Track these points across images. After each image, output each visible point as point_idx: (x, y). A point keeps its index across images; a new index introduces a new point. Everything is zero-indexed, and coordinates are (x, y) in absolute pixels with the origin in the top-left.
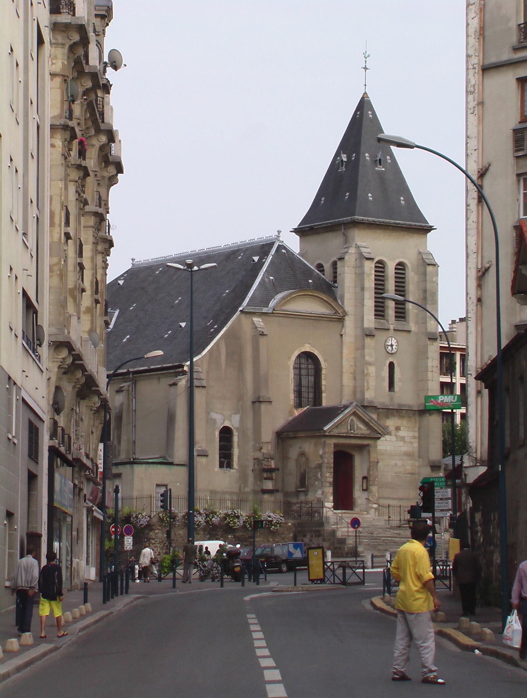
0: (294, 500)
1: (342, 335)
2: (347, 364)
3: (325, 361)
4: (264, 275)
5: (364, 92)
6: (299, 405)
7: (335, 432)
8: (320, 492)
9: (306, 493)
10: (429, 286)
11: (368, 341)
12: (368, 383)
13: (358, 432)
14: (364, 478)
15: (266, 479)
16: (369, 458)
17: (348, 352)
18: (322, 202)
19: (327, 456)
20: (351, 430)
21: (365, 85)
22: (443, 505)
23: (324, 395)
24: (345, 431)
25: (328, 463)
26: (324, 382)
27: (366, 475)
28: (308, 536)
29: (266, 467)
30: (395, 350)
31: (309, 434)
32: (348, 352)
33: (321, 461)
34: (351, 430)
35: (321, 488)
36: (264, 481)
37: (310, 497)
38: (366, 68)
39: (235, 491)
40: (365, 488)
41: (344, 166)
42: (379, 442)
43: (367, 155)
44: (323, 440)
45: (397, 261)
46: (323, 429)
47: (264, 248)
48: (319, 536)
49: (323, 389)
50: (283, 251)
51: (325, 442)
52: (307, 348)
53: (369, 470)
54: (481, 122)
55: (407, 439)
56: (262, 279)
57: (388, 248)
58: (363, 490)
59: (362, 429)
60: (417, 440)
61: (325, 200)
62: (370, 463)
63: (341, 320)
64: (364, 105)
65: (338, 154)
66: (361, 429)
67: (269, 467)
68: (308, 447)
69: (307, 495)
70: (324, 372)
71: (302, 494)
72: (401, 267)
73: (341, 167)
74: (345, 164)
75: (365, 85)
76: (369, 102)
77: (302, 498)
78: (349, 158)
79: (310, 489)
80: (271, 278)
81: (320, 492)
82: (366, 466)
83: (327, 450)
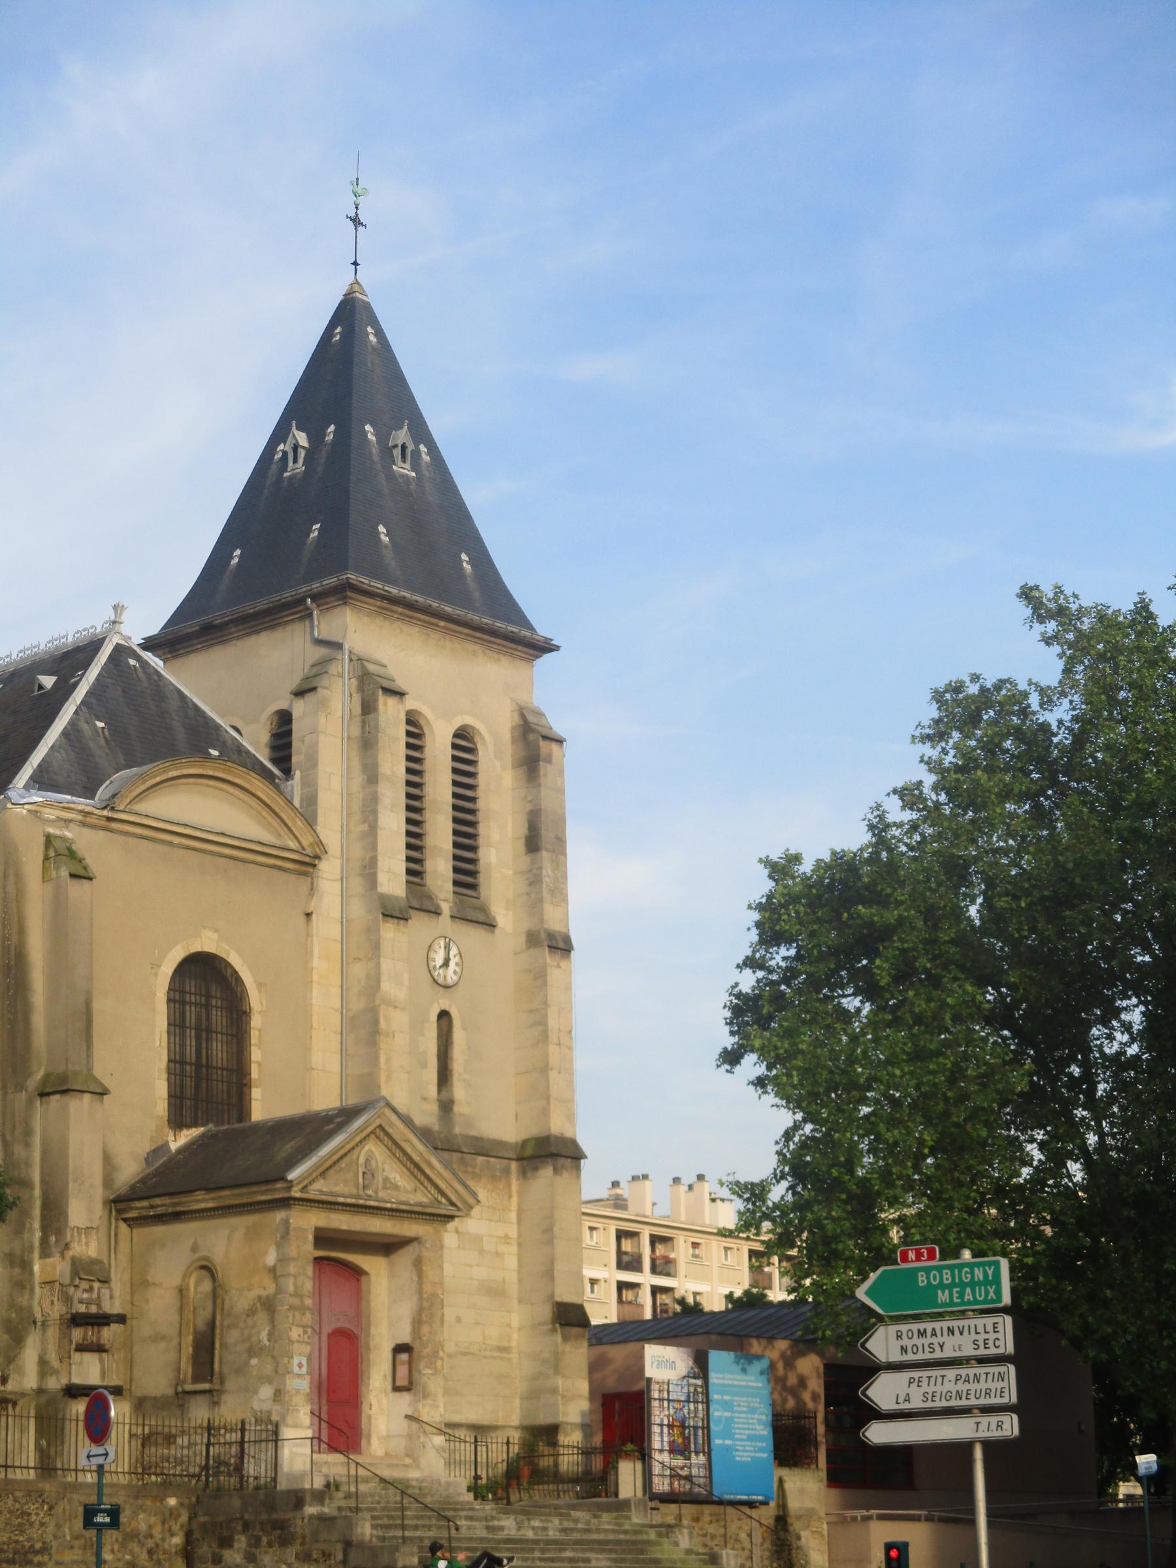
0: (172, 1423)
1: (308, 915)
2: (325, 1002)
3: (260, 986)
4: (76, 712)
5: (352, 280)
6: (177, 1121)
7: (319, 1188)
8: (266, 1392)
9: (213, 1396)
10: (547, 799)
11: (389, 932)
12: (388, 1059)
13: (390, 1198)
14: (399, 1349)
15: (81, 1348)
16: (420, 1282)
17: (324, 966)
18: (236, 560)
19: (292, 1269)
20: (365, 1187)
21: (355, 264)
22: (983, 1385)
23: (256, 1093)
24: (349, 1189)
25: (297, 1294)
26: (256, 1054)
27: (405, 1337)
28: (241, 1542)
29: (82, 1309)
30: (455, 978)
31: (228, 1197)
32: (324, 966)
33: (271, 1289)
34: (365, 1187)
35: (270, 1381)
36: (77, 1356)
37: (230, 1410)
38: (356, 221)
39: (457, 1130)
40: (402, 1381)
41: (301, 461)
42: (449, 1236)
43: (368, 428)
44: (279, 1216)
45: (457, 723)
46: (283, 1179)
47: (71, 660)
48: (285, 1542)
49: (254, 1074)
50: (132, 662)
51: (286, 1223)
52: (207, 943)
53: (417, 1323)
55: (488, 1245)
56: (72, 723)
57: (442, 680)
58: (396, 1389)
59: (400, 1186)
60: (514, 1249)
61: (241, 556)
62: (421, 1299)
63: (307, 865)
64: (351, 314)
65: (280, 433)
66: (397, 1188)
67: (93, 1309)
68: (223, 1240)
69: (216, 1404)
70: (256, 1021)
71: (201, 1399)
72: (464, 744)
73: (291, 464)
74: (302, 454)
75: (355, 264)
76: (367, 307)
77: (199, 1413)
78: (316, 438)
79: (230, 1385)
80: (101, 725)
81: (266, 1392)
82: (406, 1310)
83: (292, 1250)
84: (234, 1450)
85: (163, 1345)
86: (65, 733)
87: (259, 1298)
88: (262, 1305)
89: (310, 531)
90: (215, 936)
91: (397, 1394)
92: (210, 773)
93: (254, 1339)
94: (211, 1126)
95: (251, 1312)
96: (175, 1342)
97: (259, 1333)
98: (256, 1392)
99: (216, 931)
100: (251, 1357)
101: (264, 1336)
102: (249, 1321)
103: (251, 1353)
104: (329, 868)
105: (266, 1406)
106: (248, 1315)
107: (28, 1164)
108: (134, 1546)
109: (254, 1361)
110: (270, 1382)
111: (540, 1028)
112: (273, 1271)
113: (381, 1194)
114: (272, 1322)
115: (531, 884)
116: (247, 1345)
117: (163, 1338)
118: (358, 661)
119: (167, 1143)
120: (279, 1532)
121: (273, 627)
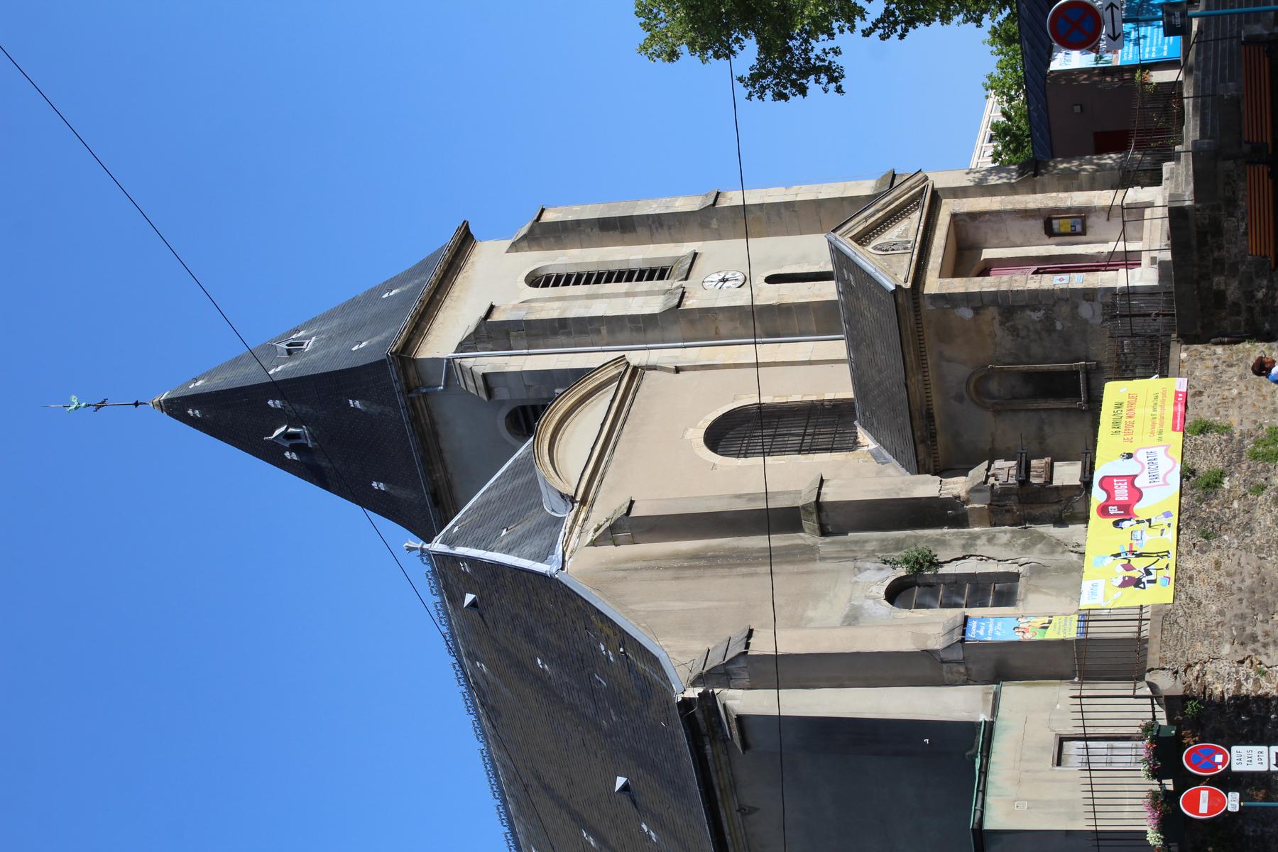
1: (678, 370)
3: (735, 399)
6: (854, 445)
28: (1218, 281)
54: (653, 563)
84: (1139, 342)
85: (1047, 429)
86: (509, 552)
87: (1002, 324)
88: (1008, 321)
89: (355, 408)
90: (691, 430)
91: (1089, 231)
92: (548, 435)
93: (1039, 326)
94: (856, 423)
95: (1014, 331)
96: (1044, 415)
97: (1033, 322)
98: (1086, 322)
99: (686, 429)
100: (1055, 330)
101: (1036, 316)
102: (1023, 333)
103: (1050, 330)
104: (636, 357)
105: (1098, 308)
106: (1018, 335)
107: (883, 540)
108: (1224, 377)
109: (1059, 326)
110: (1076, 307)
111: (783, 210)
112: (977, 310)
113: (912, 238)
114: (1023, 308)
115: (661, 226)
116: (1044, 334)
117: (1041, 429)
118: (463, 346)
119: (870, 452)
120: (1209, 238)
121: (436, 435)
